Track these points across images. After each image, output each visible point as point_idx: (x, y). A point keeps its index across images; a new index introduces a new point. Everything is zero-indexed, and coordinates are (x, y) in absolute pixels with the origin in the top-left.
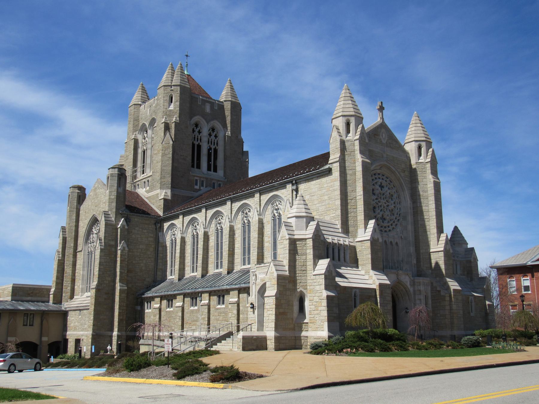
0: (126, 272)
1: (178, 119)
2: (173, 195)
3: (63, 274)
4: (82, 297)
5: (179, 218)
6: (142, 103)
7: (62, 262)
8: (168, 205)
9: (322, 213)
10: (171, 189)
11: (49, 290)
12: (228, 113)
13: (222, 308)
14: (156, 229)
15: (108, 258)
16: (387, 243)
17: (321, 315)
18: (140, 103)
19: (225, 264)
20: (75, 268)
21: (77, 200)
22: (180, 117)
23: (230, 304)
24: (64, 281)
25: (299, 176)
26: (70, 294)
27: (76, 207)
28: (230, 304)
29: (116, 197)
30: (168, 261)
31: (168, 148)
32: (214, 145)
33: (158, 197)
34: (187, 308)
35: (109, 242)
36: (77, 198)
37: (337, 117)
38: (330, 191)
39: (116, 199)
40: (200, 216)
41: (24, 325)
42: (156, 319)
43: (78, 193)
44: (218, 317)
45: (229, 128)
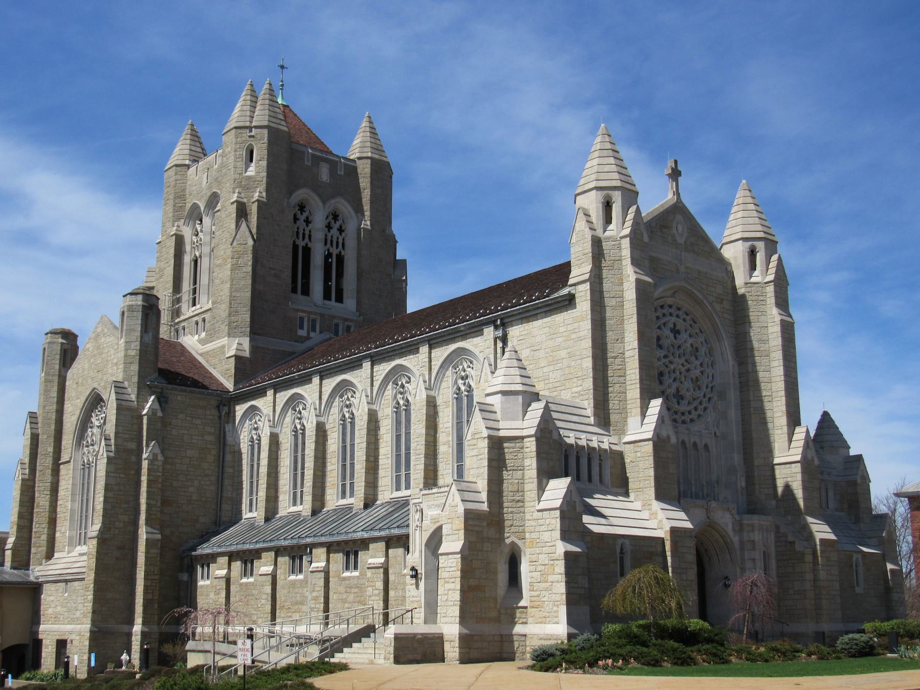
0: (159, 504)
1: (264, 194)
2: (254, 348)
6: (191, 163)
7: (30, 483)
9: (556, 385)
12: (365, 183)
13: (354, 577)
14: (220, 417)
15: (122, 476)
16: (699, 446)
17: (554, 591)
18: (187, 162)
19: (360, 488)
20: (57, 496)
23: (368, 568)
24: (34, 524)
26: (45, 548)
27: (57, 373)
28: (368, 568)
29: (138, 352)
30: (244, 483)
31: (245, 253)
32: (337, 247)
33: (224, 353)
34: (282, 577)
36: (61, 355)
38: (572, 341)
39: (138, 357)
42: (221, 600)
44: (345, 596)
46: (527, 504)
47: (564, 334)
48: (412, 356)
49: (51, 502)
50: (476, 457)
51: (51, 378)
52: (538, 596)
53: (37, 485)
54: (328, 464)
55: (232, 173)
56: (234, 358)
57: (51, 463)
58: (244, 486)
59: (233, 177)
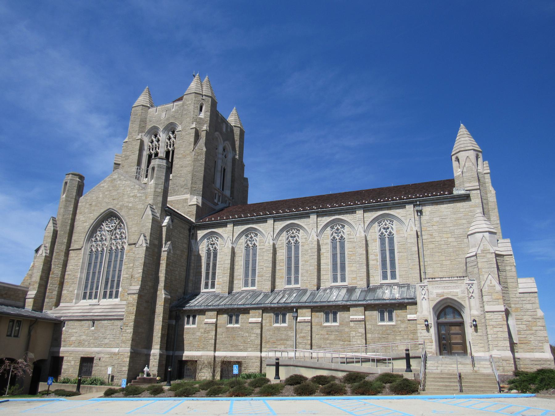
1: (208, 128)
2: (203, 203)
3: (49, 274)
4: (76, 305)
5: (227, 227)
6: (150, 106)
7: (49, 259)
8: (200, 212)
10: (202, 197)
11: (25, 293)
12: (237, 138)
13: (334, 326)
14: (190, 235)
18: (149, 105)
20: (66, 269)
21: (77, 190)
22: (210, 127)
23: (351, 321)
24: (49, 284)
25: (425, 198)
27: (74, 197)
28: (351, 321)
29: (163, 190)
30: (203, 272)
31: (201, 154)
33: (186, 202)
35: (154, 241)
36: (77, 187)
37: (466, 150)
39: (162, 193)
40: (262, 226)
41: (7, 336)
43: (79, 181)
44: (327, 336)
45: (237, 152)
46: (510, 289)
47: (463, 212)
48: (349, 215)
49: (62, 272)
50: (486, 263)
51: (70, 199)
52: (525, 338)
53: (53, 261)
54: (277, 266)
55: (192, 114)
56: (196, 206)
57: (65, 248)
58: (203, 274)
59: (192, 116)
